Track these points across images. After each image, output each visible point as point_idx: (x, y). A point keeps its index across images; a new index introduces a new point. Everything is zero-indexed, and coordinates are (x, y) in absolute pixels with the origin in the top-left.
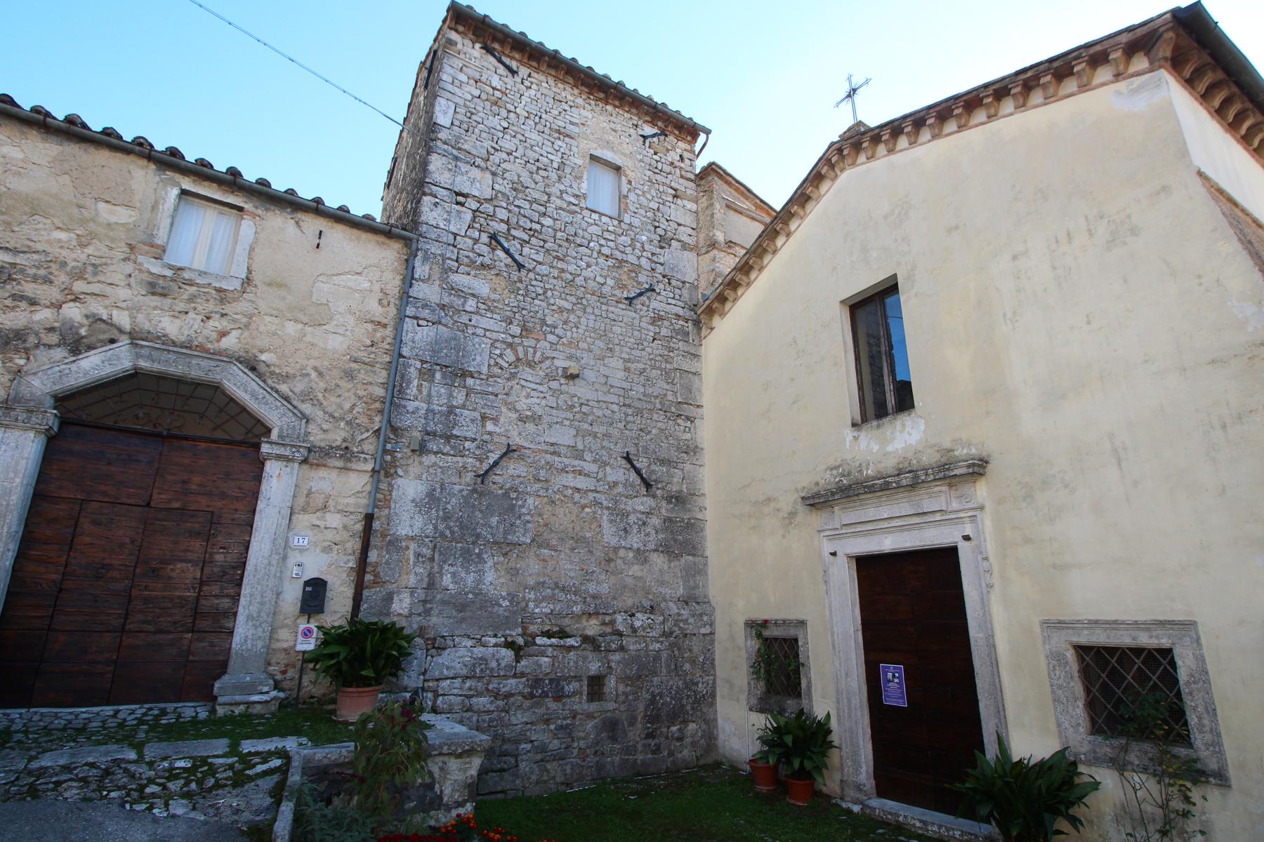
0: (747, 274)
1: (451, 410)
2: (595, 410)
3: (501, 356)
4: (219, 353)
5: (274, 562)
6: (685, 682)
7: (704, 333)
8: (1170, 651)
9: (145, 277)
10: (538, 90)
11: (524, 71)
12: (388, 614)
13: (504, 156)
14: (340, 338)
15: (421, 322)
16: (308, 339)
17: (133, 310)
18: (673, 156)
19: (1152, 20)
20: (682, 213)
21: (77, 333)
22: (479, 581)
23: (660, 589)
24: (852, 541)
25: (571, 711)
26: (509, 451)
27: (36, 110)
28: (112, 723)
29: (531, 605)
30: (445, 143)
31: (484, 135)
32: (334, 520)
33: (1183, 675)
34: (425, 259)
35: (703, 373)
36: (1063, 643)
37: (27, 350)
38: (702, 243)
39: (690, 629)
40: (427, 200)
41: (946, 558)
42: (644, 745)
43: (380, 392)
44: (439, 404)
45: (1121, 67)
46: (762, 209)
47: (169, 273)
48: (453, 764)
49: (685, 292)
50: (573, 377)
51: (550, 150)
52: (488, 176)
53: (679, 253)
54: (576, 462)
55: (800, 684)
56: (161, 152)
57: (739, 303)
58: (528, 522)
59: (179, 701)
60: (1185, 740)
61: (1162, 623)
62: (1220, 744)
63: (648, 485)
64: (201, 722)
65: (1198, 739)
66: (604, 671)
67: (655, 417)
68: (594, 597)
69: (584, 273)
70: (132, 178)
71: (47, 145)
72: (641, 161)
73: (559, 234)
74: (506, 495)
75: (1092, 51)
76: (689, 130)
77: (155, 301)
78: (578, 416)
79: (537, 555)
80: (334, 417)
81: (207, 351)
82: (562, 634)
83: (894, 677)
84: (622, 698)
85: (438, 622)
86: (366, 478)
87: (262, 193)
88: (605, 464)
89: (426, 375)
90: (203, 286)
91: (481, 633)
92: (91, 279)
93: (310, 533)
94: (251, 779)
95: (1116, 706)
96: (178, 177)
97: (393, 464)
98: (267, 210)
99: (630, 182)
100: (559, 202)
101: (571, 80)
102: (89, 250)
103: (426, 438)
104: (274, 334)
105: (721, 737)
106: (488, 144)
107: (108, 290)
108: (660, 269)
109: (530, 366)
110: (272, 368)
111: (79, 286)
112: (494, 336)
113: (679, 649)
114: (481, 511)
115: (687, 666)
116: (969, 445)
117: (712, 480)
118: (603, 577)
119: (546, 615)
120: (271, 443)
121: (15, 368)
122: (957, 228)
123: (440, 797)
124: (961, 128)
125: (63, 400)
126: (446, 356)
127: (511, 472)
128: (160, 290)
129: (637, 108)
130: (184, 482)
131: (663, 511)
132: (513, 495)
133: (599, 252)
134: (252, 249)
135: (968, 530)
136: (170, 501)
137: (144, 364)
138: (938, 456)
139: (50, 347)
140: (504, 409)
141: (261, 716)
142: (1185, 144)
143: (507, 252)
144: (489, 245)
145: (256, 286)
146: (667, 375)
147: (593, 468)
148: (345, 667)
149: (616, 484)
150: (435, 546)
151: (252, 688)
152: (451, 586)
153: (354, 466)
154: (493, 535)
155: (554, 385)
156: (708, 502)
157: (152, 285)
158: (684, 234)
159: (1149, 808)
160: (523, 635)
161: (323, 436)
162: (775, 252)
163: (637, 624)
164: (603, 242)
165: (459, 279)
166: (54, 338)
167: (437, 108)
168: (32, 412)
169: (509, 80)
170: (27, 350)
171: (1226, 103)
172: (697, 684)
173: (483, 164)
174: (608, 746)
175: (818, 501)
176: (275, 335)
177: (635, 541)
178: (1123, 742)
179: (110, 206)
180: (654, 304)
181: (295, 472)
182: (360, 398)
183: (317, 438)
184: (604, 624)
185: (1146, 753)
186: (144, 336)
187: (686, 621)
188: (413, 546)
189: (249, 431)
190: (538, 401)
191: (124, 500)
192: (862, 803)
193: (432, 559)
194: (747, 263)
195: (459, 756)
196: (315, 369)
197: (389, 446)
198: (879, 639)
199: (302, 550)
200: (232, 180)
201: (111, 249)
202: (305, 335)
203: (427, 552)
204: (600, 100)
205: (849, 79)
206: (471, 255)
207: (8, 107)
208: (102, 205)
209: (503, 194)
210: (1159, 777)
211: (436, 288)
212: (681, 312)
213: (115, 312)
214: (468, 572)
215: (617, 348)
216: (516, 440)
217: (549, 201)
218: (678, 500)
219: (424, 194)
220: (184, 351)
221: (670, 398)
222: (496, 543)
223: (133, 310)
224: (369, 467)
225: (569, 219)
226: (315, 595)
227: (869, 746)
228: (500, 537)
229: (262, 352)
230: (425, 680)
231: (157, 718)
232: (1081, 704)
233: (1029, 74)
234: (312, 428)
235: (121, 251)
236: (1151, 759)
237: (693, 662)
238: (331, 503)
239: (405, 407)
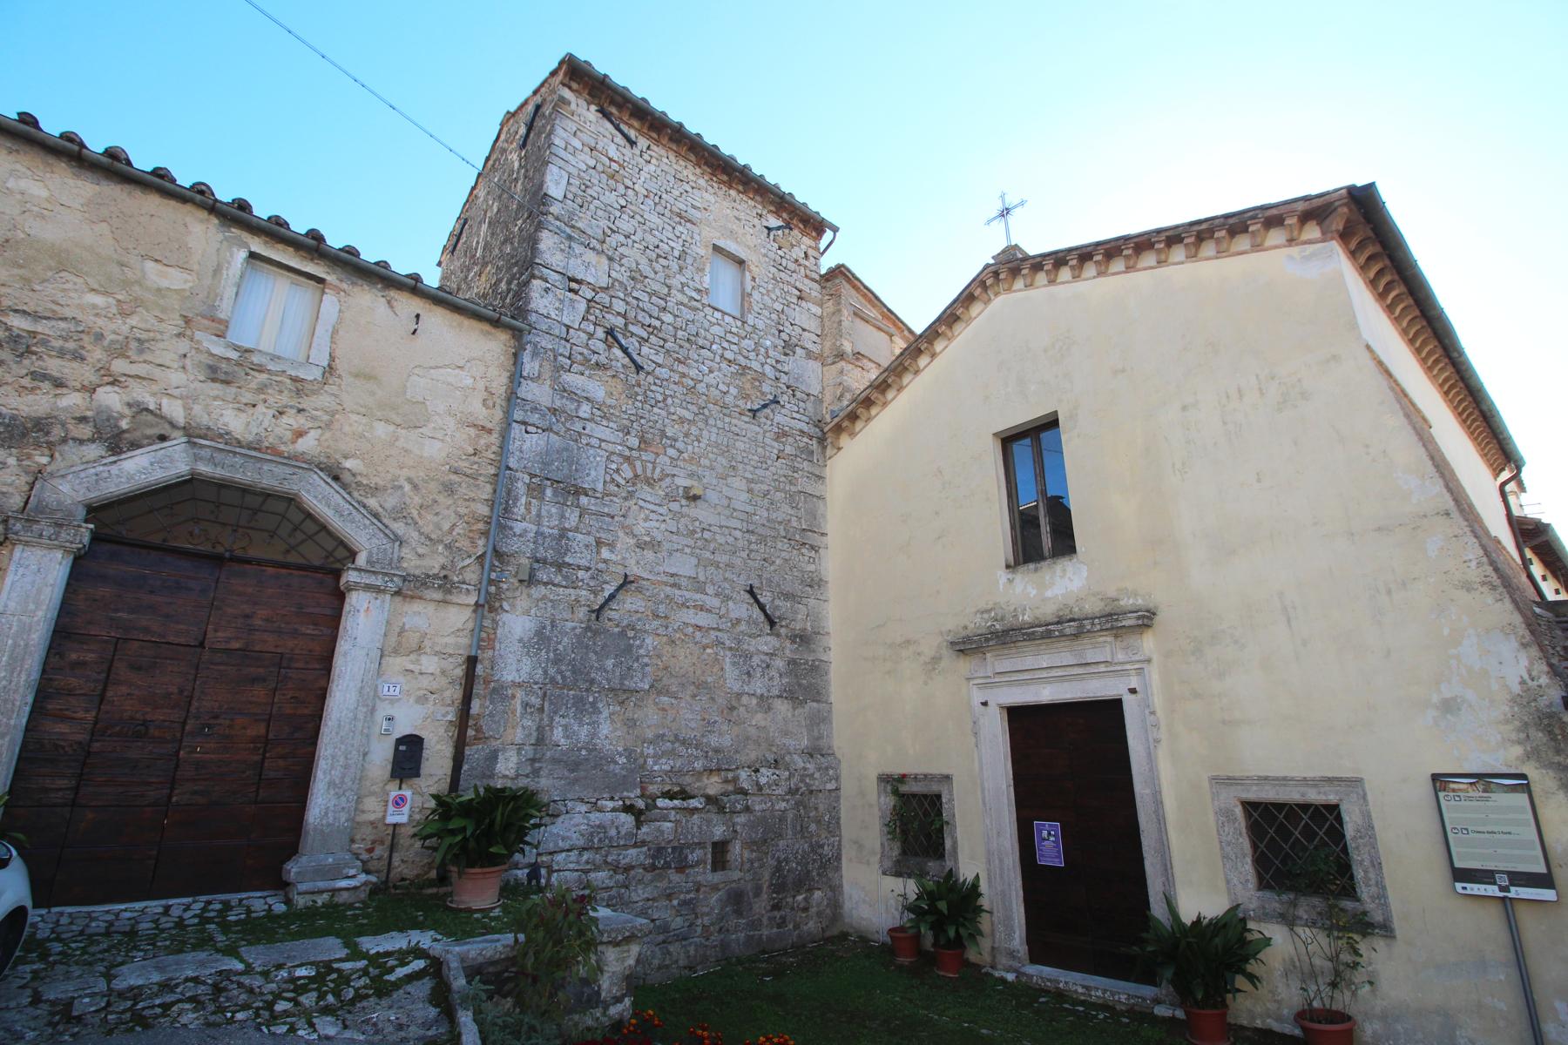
0: (883, 392)
1: (563, 533)
3: (617, 471)
4: (294, 457)
5: (361, 716)
7: (829, 452)
8: (1337, 806)
9: (204, 358)
10: (657, 166)
11: (643, 143)
12: (492, 776)
13: (622, 238)
14: (438, 444)
15: (530, 429)
18: (798, 253)
19: (1328, 193)
20: (806, 317)
21: (117, 426)
22: (594, 735)
25: (694, 882)
26: (626, 582)
27: (68, 137)
28: (166, 922)
29: (650, 761)
31: (600, 213)
32: (430, 664)
33: (1349, 831)
34: (535, 354)
35: (828, 496)
36: (1231, 799)
37: (51, 445)
39: (816, 785)
43: (484, 510)
44: (550, 526)
46: (888, 318)
47: (234, 355)
48: (611, 954)
49: (809, 405)
51: (671, 236)
52: (605, 261)
54: (698, 596)
55: (943, 844)
56: (227, 204)
57: (873, 424)
59: (246, 891)
60: (1350, 891)
61: (1330, 780)
62: (1385, 897)
63: (772, 623)
64: (278, 916)
65: (1365, 892)
66: (728, 835)
67: (779, 545)
68: (717, 751)
69: (706, 379)
71: (80, 183)
72: (765, 255)
73: (680, 333)
74: (623, 633)
76: (815, 225)
77: (216, 389)
78: (699, 543)
79: (656, 704)
81: (280, 454)
82: (684, 795)
83: (1049, 838)
84: (747, 866)
86: (467, 613)
87: (349, 263)
88: (728, 598)
89: (535, 491)
90: (276, 373)
92: (134, 358)
93: (401, 679)
94: (396, 986)
95: (1283, 862)
96: (246, 236)
97: (498, 596)
98: (353, 284)
99: (754, 279)
100: (680, 297)
101: (693, 158)
102: (133, 321)
103: (536, 565)
104: (362, 436)
105: (847, 905)
106: (604, 223)
107: (157, 373)
108: (784, 378)
109: (649, 484)
110: (359, 478)
111: (119, 366)
112: (610, 447)
114: (596, 653)
115: (813, 827)
117: (838, 618)
118: (725, 727)
119: (666, 772)
120: (359, 570)
121: (34, 468)
122: (1123, 371)
123: (598, 993)
125: (95, 511)
126: (558, 470)
127: (628, 606)
128: (223, 377)
130: (247, 616)
131: (787, 652)
132: (631, 634)
134: (335, 332)
136: (228, 640)
137: (204, 469)
139: (81, 442)
140: (621, 534)
141: (351, 906)
142: (1354, 316)
143: (625, 350)
145: (340, 377)
146: (791, 499)
147: (716, 602)
148: (472, 844)
149: (738, 621)
151: (336, 872)
153: (454, 598)
154: (609, 681)
155: (675, 506)
156: (833, 642)
157: (213, 369)
158: (809, 340)
160: (642, 796)
162: (917, 372)
163: (763, 780)
164: (726, 345)
166: (86, 431)
167: (548, 178)
168: (61, 526)
169: (627, 151)
170: (51, 445)
171: (1380, 273)
172: (822, 846)
174: (733, 921)
175: (967, 646)
176: (359, 435)
177: (758, 686)
178: (1292, 896)
179: (159, 267)
180: (778, 418)
183: (412, 564)
184: (726, 781)
185: (1314, 907)
188: (520, 694)
189: (330, 554)
191: (171, 639)
193: (541, 710)
194: (885, 381)
195: (617, 944)
196: (409, 480)
197: (493, 576)
198: (1033, 796)
200: (313, 245)
201: (161, 321)
205: (1002, 197)
206: (585, 351)
207: (33, 130)
208: (150, 265)
209: (621, 283)
210: (1329, 931)
211: (547, 387)
212: (805, 428)
213: (165, 401)
214: (581, 724)
215: (741, 466)
216: (634, 570)
217: (669, 295)
218: (803, 639)
219: (533, 276)
222: (612, 690)
223: (188, 399)
224: (472, 600)
225: (690, 316)
227: (1022, 910)
228: (616, 683)
229: (346, 458)
232: (1249, 860)
233: (1204, 226)
235: (173, 324)
236: (1320, 914)
238: (427, 643)
239: (511, 528)
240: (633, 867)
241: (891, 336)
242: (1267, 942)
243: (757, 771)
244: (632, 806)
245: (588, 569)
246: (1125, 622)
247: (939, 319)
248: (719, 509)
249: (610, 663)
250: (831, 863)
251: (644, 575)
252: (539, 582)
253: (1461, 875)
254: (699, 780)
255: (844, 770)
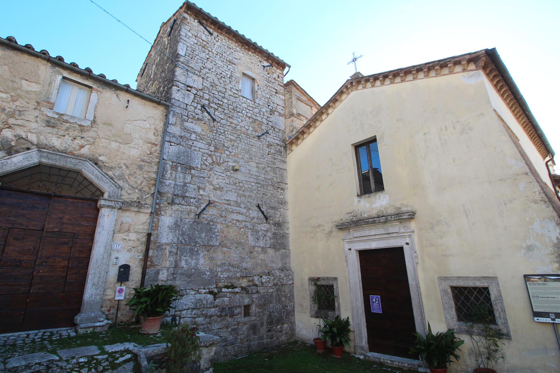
1: (185, 184)
2: (245, 185)
3: (206, 160)
4: (80, 156)
5: (105, 257)
6: (283, 306)
7: (288, 152)
9: (44, 117)
10: (221, 43)
11: (215, 34)
12: (157, 280)
13: (207, 71)
14: (136, 150)
15: (172, 144)
16: (121, 150)
17: (38, 134)
20: (279, 100)
21: (10, 144)
22: (197, 264)
23: (272, 265)
24: (362, 244)
25: (237, 322)
26: (210, 203)
29: (219, 274)
30: (182, 63)
31: (199, 61)
32: (133, 236)
33: (493, 297)
35: (288, 169)
36: (446, 286)
38: (287, 114)
39: (284, 282)
40: (174, 88)
41: (399, 251)
42: (267, 335)
43: (154, 176)
44: (180, 182)
45: (466, 67)
46: (310, 100)
47: (56, 116)
49: (280, 134)
50: (236, 170)
53: (278, 117)
54: (238, 208)
55: (334, 305)
56: (54, 58)
57: (305, 141)
58: (218, 236)
62: (507, 323)
63: (267, 219)
64: (73, 338)
65: (499, 321)
67: (269, 188)
68: (245, 269)
69: (241, 124)
70: (39, 69)
72: (263, 77)
73: (230, 107)
74: (208, 223)
75: (455, 60)
76: (281, 65)
77: (49, 130)
78: (238, 188)
80: (133, 187)
81: (74, 155)
82: (233, 287)
84: (258, 315)
85: (179, 283)
86: (148, 216)
87: (101, 80)
88: (249, 209)
89: (174, 168)
90: (73, 123)
91: (198, 287)
92: (17, 118)
93: (122, 243)
94: (120, 365)
96: (61, 70)
99: (258, 86)
100: (230, 93)
101: (235, 40)
102: (17, 103)
103: (174, 197)
104: (106, 147)
106: (200, 65)
107: (26, 123)
108: (270, 124)
110: (105, 164)
111: (11, 121)
112: (203, 151)
113: (280, 291)
114: (198, 231)
115: (283, 299)
116: (407, 206)
117: (292, 216)
118: (249, 260)
119: (226, 278)
120: (105, 200)
122: (401, 120)
123: (200, 366)
124: (402, 81)
127: (210, 213)
128: (52, 125)
129: (261, 54)
130: (61, 218)
131: (273, 230)
132: (211, 223)
133: (246, 115)
134: (96, 107)
135: (408, 240)
137: (44, 160)
138: (395, 210)
140: (207, 184)
141: (101, 333)
143: (209, 113)
144: (201, 110)
145: (98, 124)
146: (274, 170)
147: (244, 211)
148: (149, 308)
149: (254, 218)
150: (178, 248)
151: (95, 320)
152: (185, 266)
153: (142, 210)
155: (228, 173)
156: (290, 226)
157: (48, 122)
158: (280, 109)
159: (482, 349)
160: (216, 287)
161: (128, 196)
162: (322, 121)
163: (264, 281)
164: (248, 111)
165: (188, 125)
169: (209, 37)
172: (287, 306)
173: (198, 74)
174: (252, 337)
175: (343, 227)
176: (105, 147)
177: (261, 243)
178: (471, 324)
179: (28, 82)
180: (268, 139)
181: (116, 214)
182: (145, 178)
183: (126, 197)
184: (249, 281)
185: (480, 328)
186: (43, 146)
187: (283, 279)
188: (168, 248)
190: (222, 181)
191: (30, 227)
192: (364, 355)
193: (177, 254)
194: (309, 124)
196: (125, 164)
197: (158, 201)
199: (118, 251)
200: (88, 74)
201: (28, 103)
202: (120, 148)
203: (174, 250)
204: (246, 49)
205: (354, 54)
206: (193, 114)
208: (24, 82)
209: (207, 87)
211: (178, 128)
212: (279, 143)
213: (29, 135)
214: (192, 259)
215: (254, 158)
216: (213, 198)
217: (226, 92)
218: (279, 225)
219: (173, 85)
220: (64, 154)
221: (275, 180)
222: (204, 246)
223: (38, 134)
224: (149, 211)
225: (234, 100)
226: (124, 272)
227: (366, 330)
229: (100, 156)
230: (176, 311)
231: (50, 337)
232: (454, 309)
233: (431, 65)
234: (123, 192)
235: (33, 105)
236: (482, 330)
237: (286, 297)
238: (132, 228)
239: (165, 183)
240: (213, 316)
241: (311, 107)
242: (462, 342)
243: (261, 277)
244: (212, 291)
245: (195, 198)
246: (404, 217)
247: (330, 100)
248: (246, 174)
249: (203, 235)
250: (290, 313)
251: (217, 200)
252: (176, 204)
253: (537, 314)
254: (238, 281)
255: (295, 276)
